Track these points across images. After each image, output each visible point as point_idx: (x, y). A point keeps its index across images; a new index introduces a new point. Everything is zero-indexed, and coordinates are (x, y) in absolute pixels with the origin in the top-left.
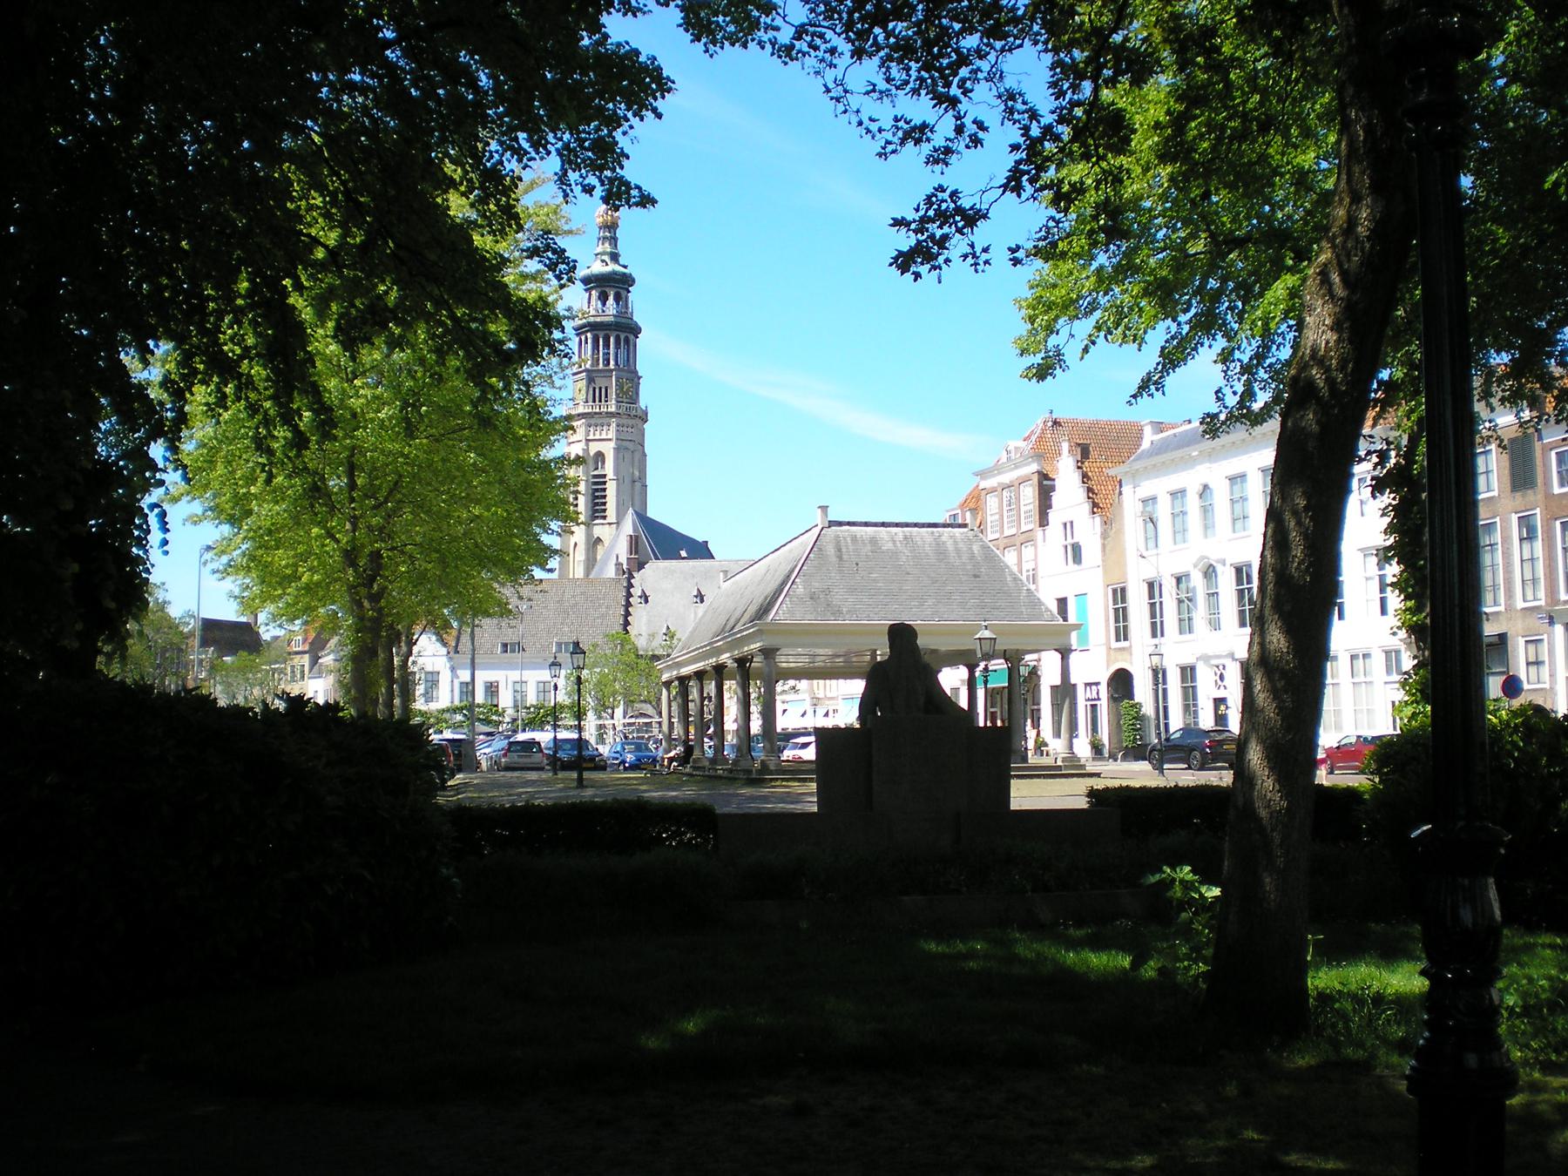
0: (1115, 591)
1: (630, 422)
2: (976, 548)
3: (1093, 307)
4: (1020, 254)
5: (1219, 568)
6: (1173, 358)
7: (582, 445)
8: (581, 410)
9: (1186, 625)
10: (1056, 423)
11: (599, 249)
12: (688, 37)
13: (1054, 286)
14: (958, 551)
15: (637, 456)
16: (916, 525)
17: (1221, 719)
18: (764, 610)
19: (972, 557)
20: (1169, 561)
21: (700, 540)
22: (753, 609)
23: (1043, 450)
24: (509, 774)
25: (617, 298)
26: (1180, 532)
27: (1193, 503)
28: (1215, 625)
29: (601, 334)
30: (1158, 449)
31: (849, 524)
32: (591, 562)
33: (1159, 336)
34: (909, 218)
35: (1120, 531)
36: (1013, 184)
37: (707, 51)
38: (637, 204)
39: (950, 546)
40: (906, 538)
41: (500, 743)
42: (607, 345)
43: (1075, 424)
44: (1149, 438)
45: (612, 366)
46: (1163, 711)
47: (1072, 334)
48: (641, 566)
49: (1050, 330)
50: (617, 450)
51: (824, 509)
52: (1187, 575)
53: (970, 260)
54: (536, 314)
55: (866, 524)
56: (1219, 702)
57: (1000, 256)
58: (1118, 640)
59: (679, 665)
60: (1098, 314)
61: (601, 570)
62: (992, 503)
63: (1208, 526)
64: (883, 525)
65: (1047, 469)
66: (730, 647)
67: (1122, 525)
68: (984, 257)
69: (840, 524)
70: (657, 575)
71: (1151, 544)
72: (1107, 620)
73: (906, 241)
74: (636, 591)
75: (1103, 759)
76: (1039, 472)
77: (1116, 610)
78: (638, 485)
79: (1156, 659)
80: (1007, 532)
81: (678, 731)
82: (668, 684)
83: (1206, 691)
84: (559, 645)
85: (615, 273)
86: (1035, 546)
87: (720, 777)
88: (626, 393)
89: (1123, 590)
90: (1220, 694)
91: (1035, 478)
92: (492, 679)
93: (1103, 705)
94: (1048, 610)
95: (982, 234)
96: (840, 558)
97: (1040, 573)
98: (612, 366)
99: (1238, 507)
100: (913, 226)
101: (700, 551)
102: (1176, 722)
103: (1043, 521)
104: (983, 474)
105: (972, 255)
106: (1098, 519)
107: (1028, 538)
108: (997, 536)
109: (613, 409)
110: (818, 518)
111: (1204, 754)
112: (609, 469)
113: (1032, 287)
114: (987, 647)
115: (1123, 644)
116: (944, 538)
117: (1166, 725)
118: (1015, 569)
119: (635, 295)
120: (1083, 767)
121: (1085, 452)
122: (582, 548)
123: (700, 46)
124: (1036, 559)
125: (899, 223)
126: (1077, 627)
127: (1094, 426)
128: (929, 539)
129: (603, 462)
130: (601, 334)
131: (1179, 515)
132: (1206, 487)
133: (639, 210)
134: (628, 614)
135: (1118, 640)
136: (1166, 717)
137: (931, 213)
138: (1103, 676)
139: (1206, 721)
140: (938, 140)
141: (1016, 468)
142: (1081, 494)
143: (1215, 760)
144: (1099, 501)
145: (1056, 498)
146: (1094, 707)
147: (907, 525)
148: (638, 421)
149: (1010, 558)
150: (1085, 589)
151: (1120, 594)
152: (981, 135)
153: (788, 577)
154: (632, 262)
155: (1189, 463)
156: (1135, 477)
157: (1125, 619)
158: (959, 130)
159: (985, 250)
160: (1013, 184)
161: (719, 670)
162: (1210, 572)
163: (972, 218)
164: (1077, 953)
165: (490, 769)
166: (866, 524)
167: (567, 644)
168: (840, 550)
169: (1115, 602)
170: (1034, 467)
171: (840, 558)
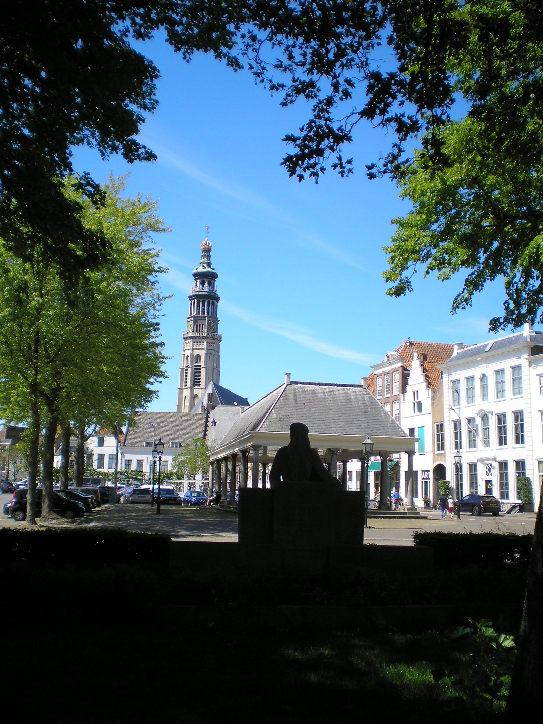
0: (438, 425)
1: (213, 341)
2: (366, 398)
3: (428, 256)
4: (374, 171)
5: (490, 416)
6: (474, 284)
7: (190, 351)
8: (190, 335)
9: (472, 444)
10: (411, 343)
11: (202, 261)
12: (173, 48)
13: (406, 240)
14: (357, 399)
15: (216, 357)
16: (335, 385)
17: (489, 491)
18: (256, 426)
19: (364, 402)
20: (467, 411)
21: (244, 398)
22: (252, 425)
23: (405, 357)
24: (132, 505)
25: (209, 284)
26: (471, 398)
27: (477, 383)
28: (487, 443)
29: (201, 300)
30: (461, 356)
31: (301, 383)
32: (192, 405)
33: (465, 272)
34: (296, 135)
35: (441, 397)
36: (368, 113)
37: (185, 58)
38: (145, 159)
39: (353, 397)
40: (330, 391)
41: (130, 489)
42: (204, 305)
43: (421, 344)
44: (456, 351)
45: (206, 315)
46: (459, 485)
47: (416, 272)
48: (213, 408)
49: (404, 268)
50: (206, 354)
51: (288, 375)
52: (474, 419)
53: (338, 169)
54: (97, 237)
55: (310, 384)
56: (488, 482)
57: (360, 171)
58: (439, 450)
59: (217, 453)
60: (430, 260)
61: (196, 410)
62: (379, 381)
63: (485, 395)
64: (319, 384)
65: (406, 365)
66: (239, 443)
67: (442, 393)
68: (348, 167)
69: (296, 383)
70: (221, 413)
71: (456, 403)
72: (433, 440)
73: (294, 151)
74: (210, 420)
75: (430, 508)
76: (402, 367)
77: (438, 435)
78: (216, 371)
79: (457, 458)
80: (386, 396)
81: (216, 488)
82: (212, 463)
83: (482, 475)
84: (173, 444)
85: (208, 272)
86: (400, 403)
87: (231, 512)
88: (212, 328)
89: (442, 425)
90: (489, 478)
91: (400, 370)
92: (141, 459)
93: (431, 481)
94: (402, 431)
95: (345, 150)
96: (296, 400)
97: (402, 415)
98: (206, 315)
99: (500, 385)
100: (298, 142)
101: (243, 402)
102: (466, 491)
103: (404, 391)
104: (375, 367)
105: (339, 165)
106: (430, 391)
107: (396, 399)
108: (381, 397)
109: (205, 335)
110: (285, 380)
111: (480, 508)
112: (202, 363)
113: (393, 241)
114: (368, 449)
115: (442, 452)
116: (350, 392)
117: (462, 493)
118: (389, 413)
119: (218, 283)
120: (418, 513)
121: (424, 358)
122: (188, 399)
123: (180, 54)
124: (399, 409)
125: (289, 138)
126: (418, 440)
127: (430, 345)
128: (342, 392)
129: (200, 360)
130: (201, 300)
131: (470, 389)
132: (484, 375)
133: (145, 163)
134: (206, 430)
135: (439, 450)
136: (462, 489)
137: (311, 134)
138: (431, 468)
139: (481, 491)
140: (323, 96)
141: (391, 364)
142: (422, 378)
143: (485, 511)
144: (432, 381)
145: (411, 380)
146: (426, 482)
147: (331, 385)
148: (217, 341)
149: (387, 408)
150: (424, 423)
151: (440, 427)
152: (350, 89)
153: (269, 409)
154: (217, 267)
155: (476, 364)
156: (450, 371)
157: (442, 440)
158: (336, 86)
159: (349, 162)
160: (368, 113)
161: (234, 455)
162: (485, 417)
163: (341, 137)
164: (395, 667)
165: (125, 502)
166: (310, 384)
167: (176, 443)
168: (296, 396)
169: (438, 431)
170: (400, 364)
171: (296, 400)
